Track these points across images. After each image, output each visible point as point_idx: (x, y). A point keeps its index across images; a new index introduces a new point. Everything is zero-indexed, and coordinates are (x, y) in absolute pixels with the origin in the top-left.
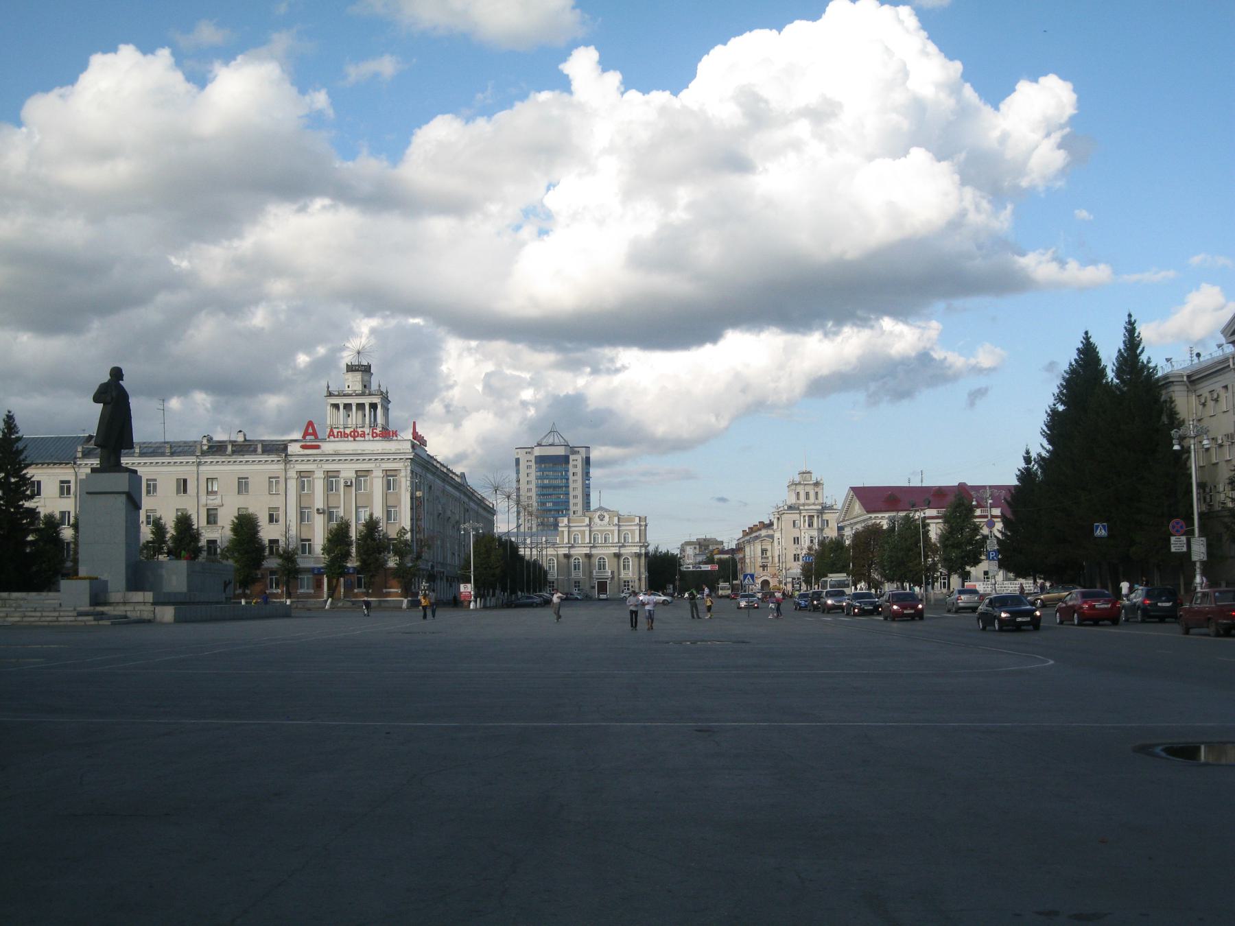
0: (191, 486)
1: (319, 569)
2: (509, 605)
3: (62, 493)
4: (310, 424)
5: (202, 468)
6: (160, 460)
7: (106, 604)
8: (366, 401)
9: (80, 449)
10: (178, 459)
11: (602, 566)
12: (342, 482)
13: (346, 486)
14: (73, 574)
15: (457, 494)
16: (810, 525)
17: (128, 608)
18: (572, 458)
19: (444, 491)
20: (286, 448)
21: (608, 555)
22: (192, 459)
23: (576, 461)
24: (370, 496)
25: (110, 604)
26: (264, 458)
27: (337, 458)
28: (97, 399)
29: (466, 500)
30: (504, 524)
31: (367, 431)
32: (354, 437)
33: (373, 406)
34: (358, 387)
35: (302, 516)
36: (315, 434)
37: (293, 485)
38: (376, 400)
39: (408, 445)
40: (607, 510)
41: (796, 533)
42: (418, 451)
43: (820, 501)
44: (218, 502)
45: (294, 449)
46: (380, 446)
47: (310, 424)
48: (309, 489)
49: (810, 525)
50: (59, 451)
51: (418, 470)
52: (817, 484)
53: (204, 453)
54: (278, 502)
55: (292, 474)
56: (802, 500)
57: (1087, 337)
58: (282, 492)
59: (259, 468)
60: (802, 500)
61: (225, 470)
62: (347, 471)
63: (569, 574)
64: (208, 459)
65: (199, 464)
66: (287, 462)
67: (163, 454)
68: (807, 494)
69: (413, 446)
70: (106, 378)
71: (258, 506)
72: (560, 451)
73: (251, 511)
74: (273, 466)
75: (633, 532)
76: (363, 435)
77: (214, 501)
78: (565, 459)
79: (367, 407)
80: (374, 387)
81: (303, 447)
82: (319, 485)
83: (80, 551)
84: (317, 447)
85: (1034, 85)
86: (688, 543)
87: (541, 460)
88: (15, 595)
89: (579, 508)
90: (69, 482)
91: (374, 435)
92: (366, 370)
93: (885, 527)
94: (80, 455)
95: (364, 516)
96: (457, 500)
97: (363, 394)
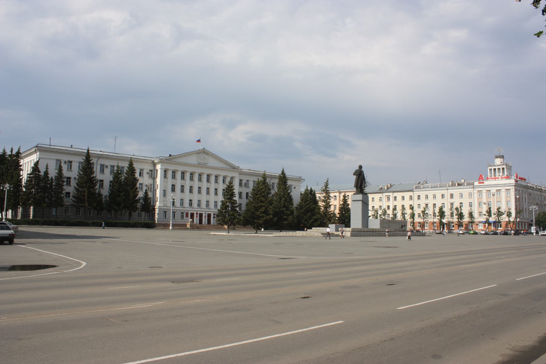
22: (446, 188)
24: (500, 197)
37: (476, 195)
55: (476, 191)
62: (493, 190)
82: (484, 195)
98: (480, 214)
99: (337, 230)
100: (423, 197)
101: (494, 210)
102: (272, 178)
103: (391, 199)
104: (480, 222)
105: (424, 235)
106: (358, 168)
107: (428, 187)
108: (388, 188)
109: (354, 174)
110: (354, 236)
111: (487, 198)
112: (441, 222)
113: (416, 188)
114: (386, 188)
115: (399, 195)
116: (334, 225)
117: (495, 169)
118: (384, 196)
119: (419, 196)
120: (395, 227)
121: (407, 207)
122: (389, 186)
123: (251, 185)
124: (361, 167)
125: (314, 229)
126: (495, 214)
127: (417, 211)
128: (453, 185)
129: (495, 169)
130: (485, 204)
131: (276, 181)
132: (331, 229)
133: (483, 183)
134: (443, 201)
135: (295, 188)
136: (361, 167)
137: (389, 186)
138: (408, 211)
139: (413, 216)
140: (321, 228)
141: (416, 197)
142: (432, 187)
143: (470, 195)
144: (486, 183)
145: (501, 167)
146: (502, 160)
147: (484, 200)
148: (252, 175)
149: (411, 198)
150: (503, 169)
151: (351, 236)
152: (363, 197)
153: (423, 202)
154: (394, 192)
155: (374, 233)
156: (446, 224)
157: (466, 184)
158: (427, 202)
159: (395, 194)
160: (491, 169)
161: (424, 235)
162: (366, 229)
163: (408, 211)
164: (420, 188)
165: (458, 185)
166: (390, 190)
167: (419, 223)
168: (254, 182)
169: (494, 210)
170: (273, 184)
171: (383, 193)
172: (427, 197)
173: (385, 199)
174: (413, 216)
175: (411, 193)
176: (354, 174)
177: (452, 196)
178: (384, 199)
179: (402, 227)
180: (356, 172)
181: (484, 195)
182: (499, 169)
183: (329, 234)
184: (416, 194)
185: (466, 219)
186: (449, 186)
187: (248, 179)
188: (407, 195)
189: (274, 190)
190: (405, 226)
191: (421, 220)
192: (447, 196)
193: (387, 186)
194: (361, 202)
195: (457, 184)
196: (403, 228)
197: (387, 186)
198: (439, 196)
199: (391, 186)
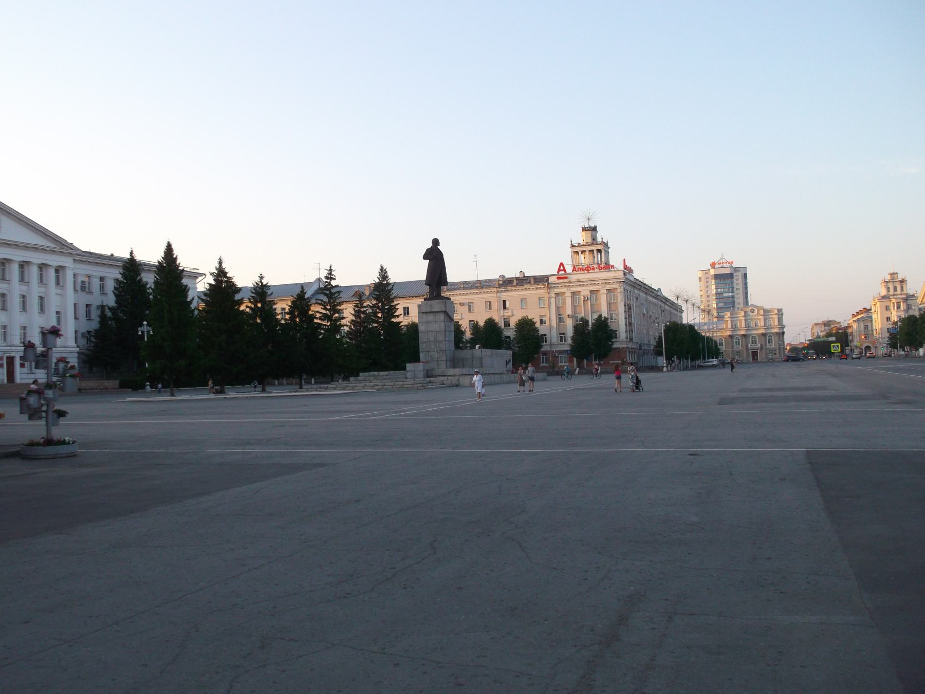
0: (494, 305)
2: (694, 368)
4: (561, 264)
7: (432, 376)
8: (594, 248)
10: (484, 290)
11: (754, 342)
13: (584, 300)
14: (416, 359)
15: (655, 301)
16: (898, 307)
17: (445, 378)
18: (735, 274)
19: (646, 300)
20: (548, 280)
21: (758, 335)
23: (738, 277)
24: (599, 305)
25: (436, 376)
28: (425, 257)
29: (662, 305)
30: (689, 317)
31: (596, 266)
33: (599, 251)
34: (590, 241)
35: (560, 319)
36: (564, 270)
38: (600, 247)
39: (621, 274)
40: (756, 307)
41: (887, 314)
42: (628, 276)
43: (905, 292)
44: (510, 314)
45: (551, 280)
46: (604, 275)
47: (561, 264)
49: (898, 307)
50: (409, 289)
51: (628, 288)
52: (902, 281)
53: (500, 286)
54: (545, 312)
56: (892, 292)
57: (169, 250)
58: (547, 306)
59: (533, 293)
60: (892, 292)
61: (512, 295)
62: (585, 291)
63: (733, 347)
67: (459, 289)
68: (895, 288)
69: (625, 274)
70: (430, 245)
71: (534, 315)
72: (728, 271)
73: (530, 317)
74: (542, 291)
75: (741, 321)
76: (593, 269)
77: (507, 313)
78: (731, 276)
80: (599, 240)
81: (558, 278)
84: (566, 278)
86: (816, 324)
87: (717, 277)
88: (382, 373)
89: (741, 306)
91: (600, 268)
92: (594, 229)
95: (596, 316)
96: (655, 304)
97: (593, 244)
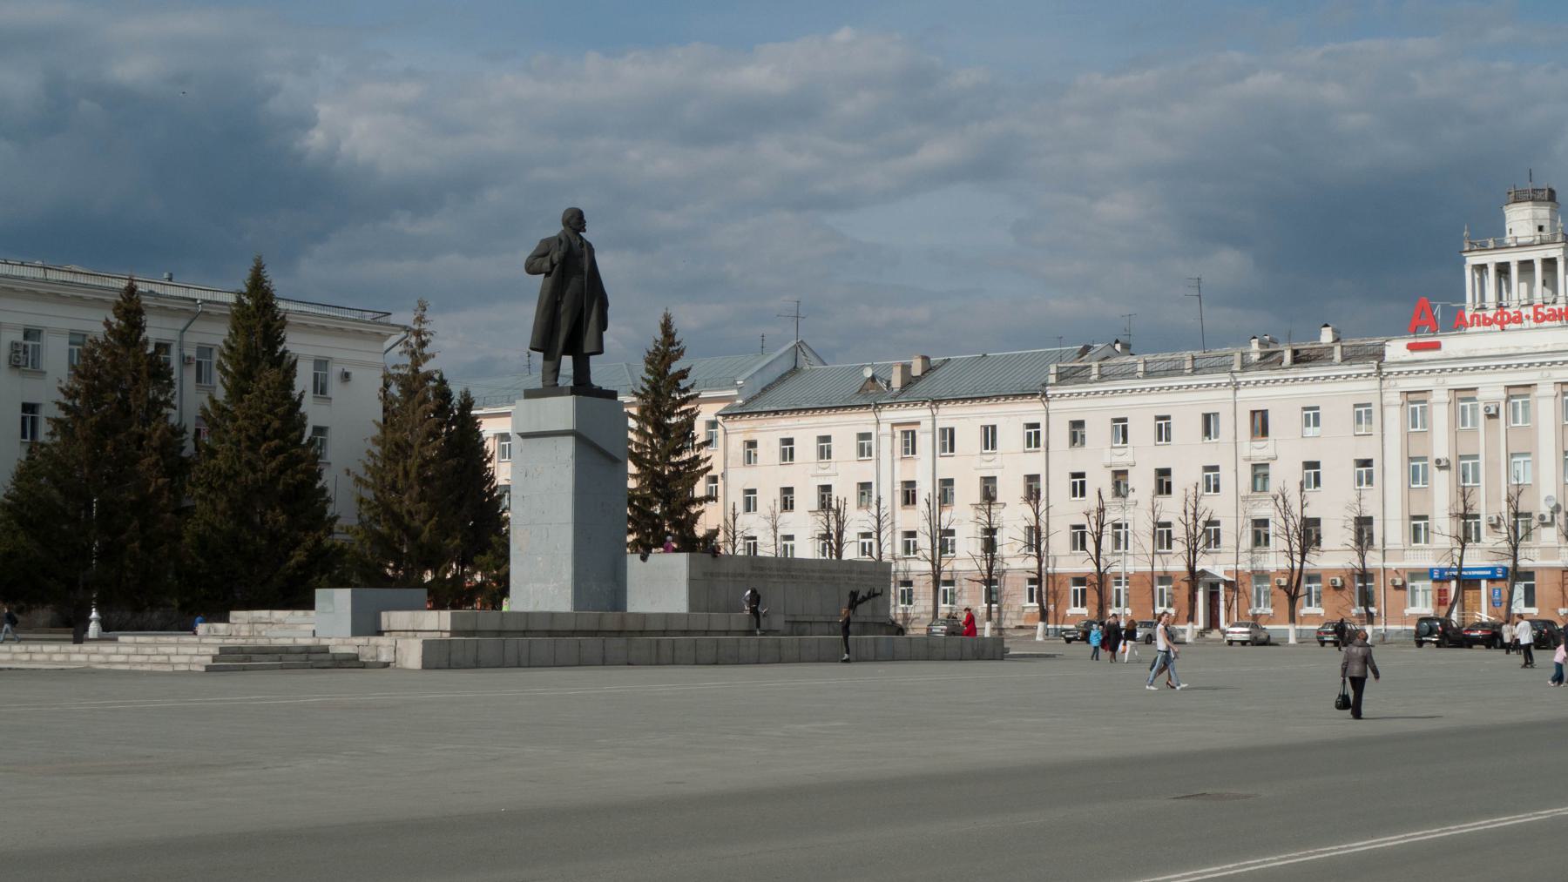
1: (1442, 570)
3: (862, 454)
5: (1241, 393)
6: (1083, 388)
9: (1053, 369)
12: (1481, 406)
22: (1225, 378)
24: (1531, 432)
26: (1345, 370)
27: (1406, 369)
32: (1502, 323)
37: (1395, 418)
48: (1526, 420)
55: (1393, 397)
62: (1491, 388)
64: (1252, 376)
65: (1237, 387)
66: (1380, 374)
79: (1538, 267)
82: (1440, 416)
83: (1465, 652)
85: (188, 638)
90: (1037, 426)
93: (184, 454)
94: (1052, 379)
98: (1418, 528)
99: (367, 624)
100: (1098, 430)
101: (1489, 504)
102: (195, 316)
103: (924, 441)
104: (1416, 575)
105: (995, 651)
106: (556, 229)
107: (1131, 374)
108: (909, 382)
109: (531, 269)
110: (450, 665)
111: (1455, 434)
112: (1191, 570)
113: (1062, 378)
114: (896, 383)
115: (967, 420)
116: (343, 596)
117: (1503, 270)
118: (886, 428)
119: (1077, 425)
120: (838, 611)
121: (1010, 490)
122: (917, 370)
123: (57, 360)
124: (575, 221)
125: (235, 615)
126: (1495, 526)
127: (1064, 511)
128: (1269, 359)
129: (1503, 270)
130: (1442, 465)
131: (217, 334)
132: (329, 618)
133: (1436, 346)
134: (1211, 452)
135: (346, 376)
136: (575, 221)
137: (917, 370)
138: (1013, 518)
139: (1035, 538)
140: (279, 614)
141: (1059, 434)
142: (1148, 374)
143: (1362, 413)
144: (1453, 345)
145: (1537, 255)
146: (1544, 212)
147: (1441, 447)
148: (58, 298)
149: (1033, 435)
150: (1550, 264)
151: (426, 665)
152: (579, 412)
153: (1097, 459)
154: (937, 402)
155: (616, 643)
156: (1226, 583)
157: (1337, 357)
158: (1121, 458)
159: (949, 415)
160: (1482, 268)
161: (995, 651)
162: (611, 621)
163: (1013, 518)
164: (1085, 380)
165: (1299, 359)
166: (920, 388)
167: (1079, 580)
168: (76, 337)
169: (1489, 504)
170: (205, 350)
171: (877, 407)
172: (1121, 429)
173: (887, 446)
174: (1035, 538)
175: (1031, 410)
176: (531, 269)
177: (1261, 424)
178: (886, 443)
179: (855, 601)
180: (543, 252)
181: (1440, 416)
182: (1526, 266)
183: (315, 659)
184: (1064, 406)
185: (1335, 555)
186: (1246, 366)
187: (33, 322)
188: (1011, 417)
189: (191, 400)
190: (873, 595)
191: (1083, 564)
192: (1236, 425)
193: (906, 368)
194: (568, 444)
195: (1288, 356)
196: (864, 610)
197: (906, 368)
198: (1186, 427)
199: (928, 369)
